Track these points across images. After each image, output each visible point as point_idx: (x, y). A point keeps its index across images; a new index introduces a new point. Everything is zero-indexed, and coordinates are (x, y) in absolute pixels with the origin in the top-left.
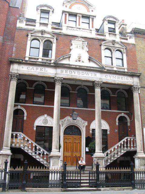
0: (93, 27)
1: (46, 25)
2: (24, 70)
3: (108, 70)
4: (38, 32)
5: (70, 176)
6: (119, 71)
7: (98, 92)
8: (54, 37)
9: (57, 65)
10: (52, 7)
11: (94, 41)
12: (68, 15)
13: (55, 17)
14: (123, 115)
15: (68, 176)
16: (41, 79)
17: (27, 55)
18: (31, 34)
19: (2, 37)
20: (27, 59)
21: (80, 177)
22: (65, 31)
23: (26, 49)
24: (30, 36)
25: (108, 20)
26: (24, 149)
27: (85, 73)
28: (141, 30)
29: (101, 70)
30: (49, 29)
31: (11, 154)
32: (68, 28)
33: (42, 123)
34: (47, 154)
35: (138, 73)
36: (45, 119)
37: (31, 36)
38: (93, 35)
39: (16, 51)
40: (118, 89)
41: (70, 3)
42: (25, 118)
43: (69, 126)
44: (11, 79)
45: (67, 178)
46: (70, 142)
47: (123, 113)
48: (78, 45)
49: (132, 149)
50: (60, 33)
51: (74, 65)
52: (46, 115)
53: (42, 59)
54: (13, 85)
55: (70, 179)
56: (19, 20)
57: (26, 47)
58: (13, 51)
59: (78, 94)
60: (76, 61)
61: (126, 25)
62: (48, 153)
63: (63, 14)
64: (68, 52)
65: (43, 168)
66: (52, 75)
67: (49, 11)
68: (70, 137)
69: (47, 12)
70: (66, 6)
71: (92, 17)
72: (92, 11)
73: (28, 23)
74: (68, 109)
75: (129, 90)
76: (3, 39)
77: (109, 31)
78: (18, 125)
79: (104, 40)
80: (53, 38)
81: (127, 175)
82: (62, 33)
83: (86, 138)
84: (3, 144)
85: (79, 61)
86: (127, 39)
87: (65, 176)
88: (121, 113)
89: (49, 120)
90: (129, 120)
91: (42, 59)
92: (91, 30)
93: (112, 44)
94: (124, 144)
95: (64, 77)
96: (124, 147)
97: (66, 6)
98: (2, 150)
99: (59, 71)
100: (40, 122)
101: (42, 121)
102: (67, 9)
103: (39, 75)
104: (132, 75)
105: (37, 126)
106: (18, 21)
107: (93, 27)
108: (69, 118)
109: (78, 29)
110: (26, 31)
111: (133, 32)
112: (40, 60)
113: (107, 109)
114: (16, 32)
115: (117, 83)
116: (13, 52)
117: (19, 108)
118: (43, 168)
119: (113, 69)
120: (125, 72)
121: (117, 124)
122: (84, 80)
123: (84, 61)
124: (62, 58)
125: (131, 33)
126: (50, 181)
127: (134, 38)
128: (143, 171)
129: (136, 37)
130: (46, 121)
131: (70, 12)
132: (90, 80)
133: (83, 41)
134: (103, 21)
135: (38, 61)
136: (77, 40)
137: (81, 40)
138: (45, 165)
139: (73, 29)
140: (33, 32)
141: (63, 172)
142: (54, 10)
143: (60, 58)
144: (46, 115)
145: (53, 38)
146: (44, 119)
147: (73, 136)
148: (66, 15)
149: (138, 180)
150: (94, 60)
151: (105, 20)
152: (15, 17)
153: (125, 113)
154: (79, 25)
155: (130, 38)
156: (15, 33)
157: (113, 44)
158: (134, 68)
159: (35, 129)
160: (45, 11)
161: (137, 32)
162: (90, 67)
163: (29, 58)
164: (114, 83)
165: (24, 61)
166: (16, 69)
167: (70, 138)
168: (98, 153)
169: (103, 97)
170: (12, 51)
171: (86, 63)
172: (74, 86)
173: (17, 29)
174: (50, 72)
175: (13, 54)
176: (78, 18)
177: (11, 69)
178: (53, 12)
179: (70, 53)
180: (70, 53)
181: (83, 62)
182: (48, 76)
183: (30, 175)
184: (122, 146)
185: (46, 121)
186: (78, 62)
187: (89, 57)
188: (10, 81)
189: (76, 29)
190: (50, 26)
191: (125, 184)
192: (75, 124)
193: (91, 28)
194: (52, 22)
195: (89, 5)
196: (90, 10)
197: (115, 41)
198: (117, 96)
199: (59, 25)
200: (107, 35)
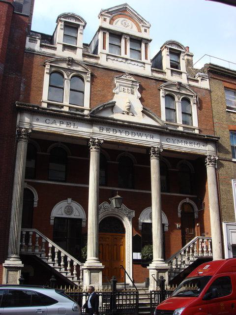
0: (146, 58)
1: (74, 49)
2: (42, 125)
3: (170, 130)
4: (63, 60)
5: (122, 299)
6: (187, 133)
7: (154, 163)
9: (94, 120)
10: (83, 18)
11: (149, 81)
12: (107, 35)
13: (85, 36)
14: (188, 200)
15: (119, 299)
16: (60, 139)
17: (45, 97)
18: (51, 62)
19: (3, 65)
20: (45, 105)
21: (121, 301)
22: (103, 61)
23: (42, 88)
24: (48, 67)
25: (170, 49)
26: (41, 256)
27: (136, 134)
28: (218, 68)
29: (161, 132)
30: (78, 56)
32: (109, 57)
33: (64, 213)
34: (78, 266)
35: (215, 137)
36: (69, 206)
37: (51, 66)
38: (147, 71)
40: (181, 159)
41: (111, 15)
42: (36, 204)
43: (108, 217)
44: (18, 138)
45: (117, 303)
46: (108, 244)
47: (187, 197)
48: (125, 88)
49: (205, 255)
50: (97, 64)
51: (120, 121)
52: (69, 200)
53: (70, 108)
54: (22, 148)
55: (122, 305)
56: (29, 38)
57: (160, 109)
59: (125, 168)
60: (124, 114)
61: (192, 56)
62: (80, 264)
63: (99, 31)
64: (109, 97)
65: (72, 288)
66: (86, 136)
67: (79, 25)
68: (107, 236)
69: (76, 27)
70: (105, 20)
71: (146, 41)
72: (145, 31)
73: (43, 44)
74: (48, 184)
75: (199, 161)
76: (5, 68)
77: (171, 66)
78: (32, 216)
79: (164, 81)
80: (87, 73)
82: (100, 65)
84: (8, 249)
85: (128, 113)
86: (197, 81)
87: (115, 301)
88: (185, 198)
89: (74, 208)
90: (196, 209)
91: (70, 108)
92: (144, 63)
94: (193, 249)
95: (105, 139)
96: (193, 252)
97: (105, 20)
99: (96, 129)
100: (59, 211)
101: (63, 211)
102: (106, 25)
103: (65, 134)
104: (206, 141)
105: (56, 218)
106: (28, 38)
107: (146, 58)
108: (106, 204)
109: (124, 61)
110: (42, 56)
111: (206, 70)
112: (66, 109)
113: (103, 185)
114: (25, 58)
115: (183, 151)
117: (188, 201)
118: (72, 288)
119: (194, 132)
121: (179, 215)
122: (136, 145)
124: (101, 108)
125: (202, 70)
126: (100, 308)
129: (210, 79)
130: (69, 210)
131: (111, 30)
132: (131, 143)
133: (133, 81)
134: (161, 48)
135: (62, 109)
136: (125, 78)
137: (129, 79)
138: (75, 283)
139: (116, 59)
140: (53, 59)
141: (111, 293)
142: (86, 24)
144: (69, 200)
145: (87, 73)
146: (68, 206)
147: (113, 234)
148: (104, 34)
150: (148, 112)
152: (22, 32)
153: (190, 198)
154: (126, 54)
155: (201, 79)
156: (23, 58)
158: (208, 128)
159: (52, 222)
160: (71, 24)
161: (215, 72)
162: (141, 124)
163: (49, 105)
164: (180, 151)
165: (40, 110)
166: (27, 122)
167: (108, 238)
168: (157, 261)
169: (30, 156)
171: (140, 118)
172: (38, 140)
174: (83, 131)
175: (21, 96)
176: (123, 41)
177: (18, 121)
178: (84, 27)
179: (112, 99)
180: (113, 100)
183: (99, 298)
184: (191, 251)
185: (69, 210)
186: (126, 115)
187: (144, 108)
188: (17, 142)
189: (121, 60)
190: (80, 52)
192: (115, 215)
193: (143, 60)
194: (84, 44)
195: (141, 21)
196: (143, 29)
197: (181, 83)
198: (50, 154)
199: (190, 77)
200: (169, 72)
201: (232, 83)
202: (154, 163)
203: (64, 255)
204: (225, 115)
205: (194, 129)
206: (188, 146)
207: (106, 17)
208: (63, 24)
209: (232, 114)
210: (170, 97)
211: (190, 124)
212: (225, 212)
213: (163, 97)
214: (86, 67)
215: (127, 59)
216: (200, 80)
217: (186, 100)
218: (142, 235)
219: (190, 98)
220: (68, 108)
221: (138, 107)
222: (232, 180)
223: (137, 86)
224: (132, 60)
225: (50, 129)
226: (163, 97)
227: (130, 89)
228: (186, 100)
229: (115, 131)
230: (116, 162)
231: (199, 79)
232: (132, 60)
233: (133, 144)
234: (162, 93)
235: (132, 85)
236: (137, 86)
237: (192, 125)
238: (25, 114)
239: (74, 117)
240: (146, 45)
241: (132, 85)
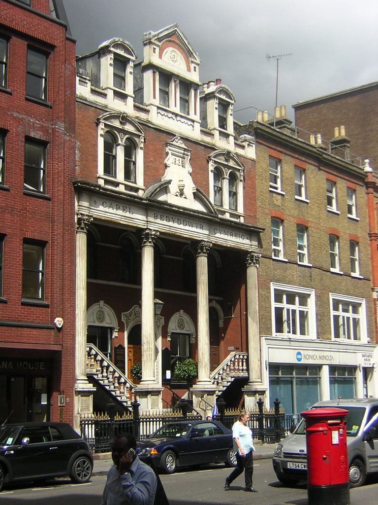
2: (106, 212)
7: (202, 263)
8: (141, 132)
23: (97, 157)
24: (102, 126)
27: (182, 222)
29: (211, 220)
31: (163, 389)
39: (82, 160)
44: (78, 228)
47: (214, 300)
52: (102, 303)
58: (77, 159)
60: (177, 195)
74: (104, 280)
81: (127, 428)
83: (162, 350)
86: (243, 147)
92: (193, 121)
93: (224, 159)
98: (140, 383)
103: (122, 222)
106: (78, 78)
116: (77, 163)
120: (239, 224)
123: (187, 197)
127: (254, 145)
128: (156, 417)
131: (162, 69)
133: (185, 150)
139: (166, 114)
143: (255, 252)
145: (140, 136)
149: (145, 436)
151: (215, 97)
155: (248, 145)
157: (227, 160)
170: (74, 161)
173: (77, 101)
174: (137, 219)
175: (77, 168)
181: (185, 198)
182: (135, 225)
189: (170, 115)
191: (105, 447)
201: (276, 150)
202: (202, 263)
203: (100, 359)
204: (268, 195)
205: (239, 216)
206: (233, 239)
207: (155, 47)
208: (112, 56)
209: (274, 195)
210: (218, 174)
211: (133, 180)
212: (264, 323)
213: (212, 171)
214: (140, 127)
215: (176, 115)
216: (246, 146)
217: (233, 179)
218: (307, 371)
219: (137, 139)
220: (103, 181)
221: (190, 188)
222: (271, 283)
223: (188, 156)
224: (182, 117)
225: (108, 215)
226: (212, 171)
227: (180, 159)
228: (233, 179)
229: (179, 221)
230: (118, 247)
231: (245, 144)
232: (182, 117)
233: (184, 236)
234: (211, 166)
235: (184, 154)
236: (188, 156)
237: (115, 177)
238: (84, 194)
239: (129, 202)
240: (196, 90)
241: (184, 154)
